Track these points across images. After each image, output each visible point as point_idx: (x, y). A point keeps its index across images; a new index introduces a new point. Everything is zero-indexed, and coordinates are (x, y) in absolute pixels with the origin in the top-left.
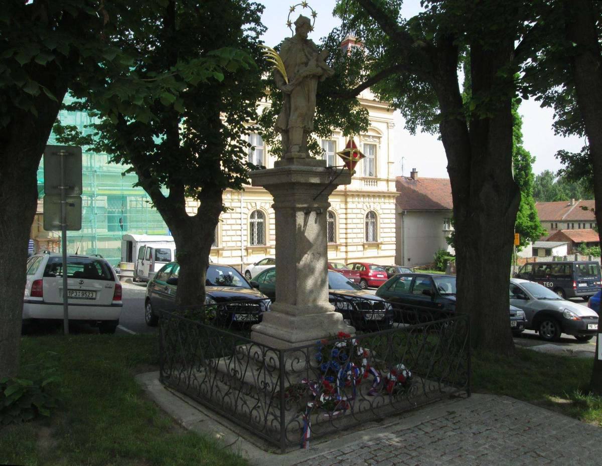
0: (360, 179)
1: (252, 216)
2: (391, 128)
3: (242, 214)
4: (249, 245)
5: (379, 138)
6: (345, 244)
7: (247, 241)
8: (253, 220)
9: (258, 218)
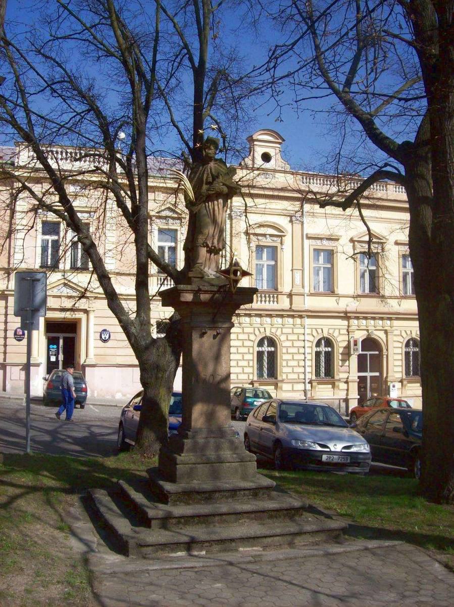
0: (354, 297)
1: (318, 344)
2: (295, 223)
3: (306, 341)
4: (314, 378)
5: (281, 236)
6: (345, 380)
7: (312, 373)
8: (260, 349)
9: (325, 346)
